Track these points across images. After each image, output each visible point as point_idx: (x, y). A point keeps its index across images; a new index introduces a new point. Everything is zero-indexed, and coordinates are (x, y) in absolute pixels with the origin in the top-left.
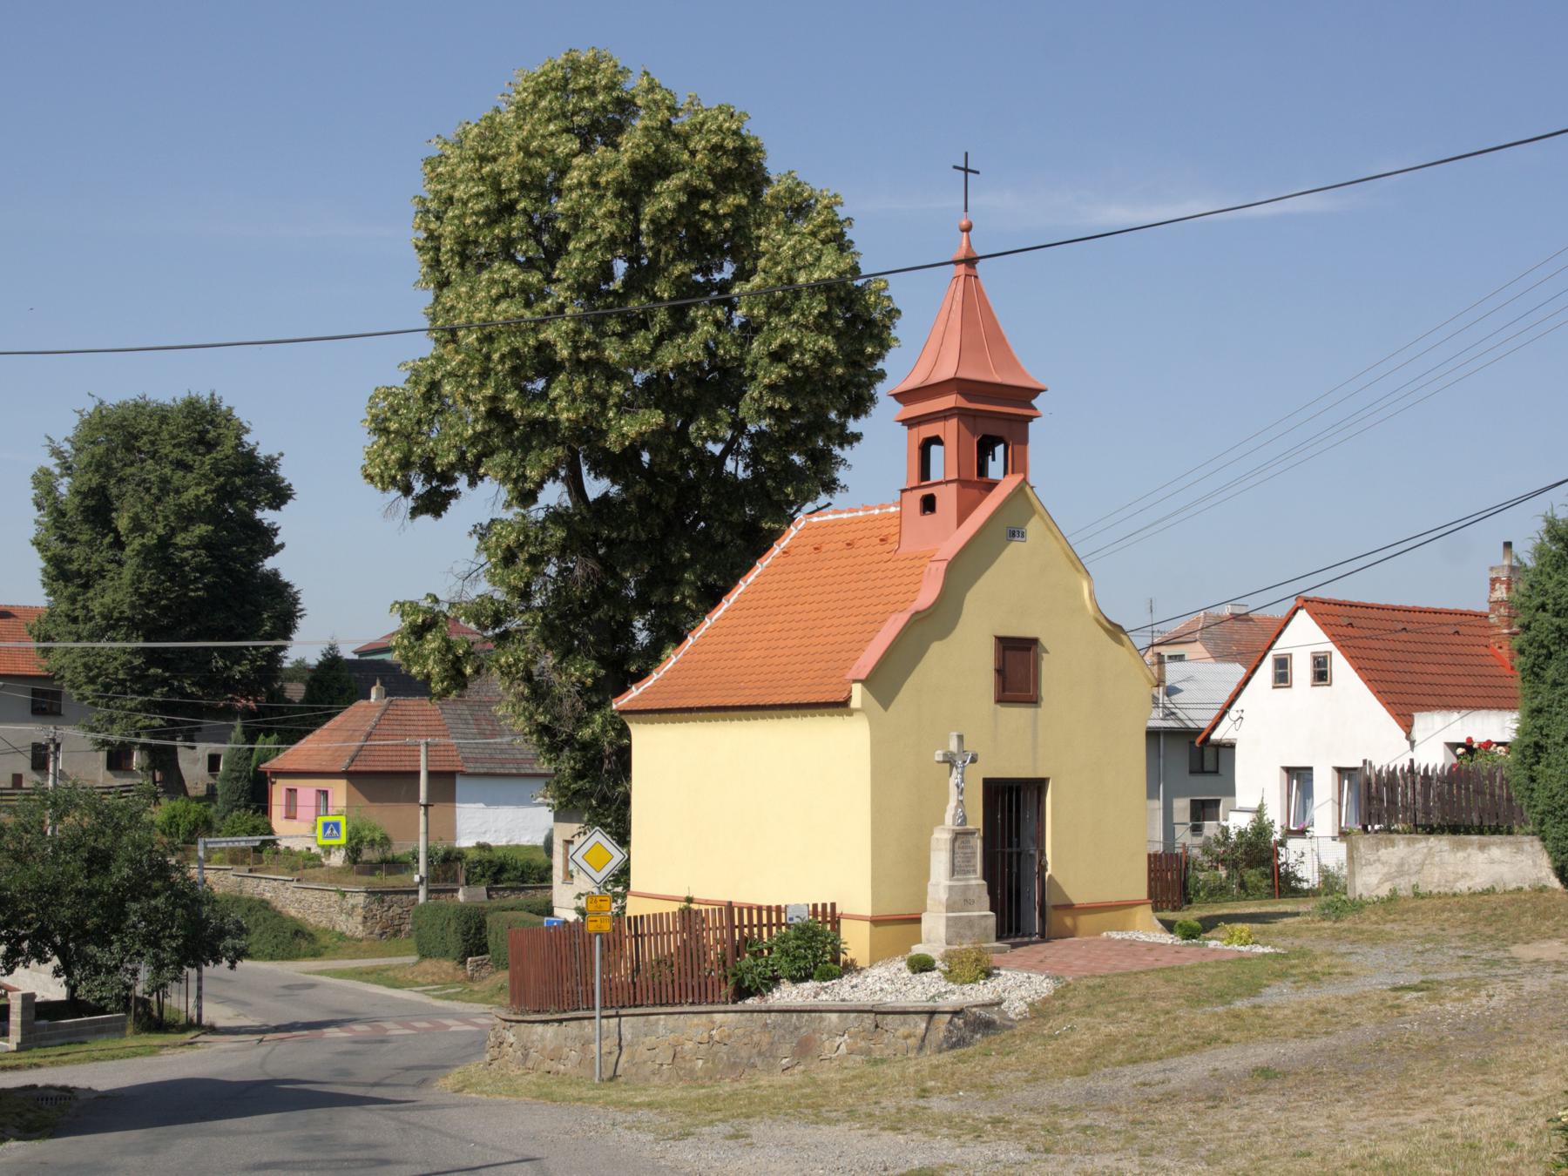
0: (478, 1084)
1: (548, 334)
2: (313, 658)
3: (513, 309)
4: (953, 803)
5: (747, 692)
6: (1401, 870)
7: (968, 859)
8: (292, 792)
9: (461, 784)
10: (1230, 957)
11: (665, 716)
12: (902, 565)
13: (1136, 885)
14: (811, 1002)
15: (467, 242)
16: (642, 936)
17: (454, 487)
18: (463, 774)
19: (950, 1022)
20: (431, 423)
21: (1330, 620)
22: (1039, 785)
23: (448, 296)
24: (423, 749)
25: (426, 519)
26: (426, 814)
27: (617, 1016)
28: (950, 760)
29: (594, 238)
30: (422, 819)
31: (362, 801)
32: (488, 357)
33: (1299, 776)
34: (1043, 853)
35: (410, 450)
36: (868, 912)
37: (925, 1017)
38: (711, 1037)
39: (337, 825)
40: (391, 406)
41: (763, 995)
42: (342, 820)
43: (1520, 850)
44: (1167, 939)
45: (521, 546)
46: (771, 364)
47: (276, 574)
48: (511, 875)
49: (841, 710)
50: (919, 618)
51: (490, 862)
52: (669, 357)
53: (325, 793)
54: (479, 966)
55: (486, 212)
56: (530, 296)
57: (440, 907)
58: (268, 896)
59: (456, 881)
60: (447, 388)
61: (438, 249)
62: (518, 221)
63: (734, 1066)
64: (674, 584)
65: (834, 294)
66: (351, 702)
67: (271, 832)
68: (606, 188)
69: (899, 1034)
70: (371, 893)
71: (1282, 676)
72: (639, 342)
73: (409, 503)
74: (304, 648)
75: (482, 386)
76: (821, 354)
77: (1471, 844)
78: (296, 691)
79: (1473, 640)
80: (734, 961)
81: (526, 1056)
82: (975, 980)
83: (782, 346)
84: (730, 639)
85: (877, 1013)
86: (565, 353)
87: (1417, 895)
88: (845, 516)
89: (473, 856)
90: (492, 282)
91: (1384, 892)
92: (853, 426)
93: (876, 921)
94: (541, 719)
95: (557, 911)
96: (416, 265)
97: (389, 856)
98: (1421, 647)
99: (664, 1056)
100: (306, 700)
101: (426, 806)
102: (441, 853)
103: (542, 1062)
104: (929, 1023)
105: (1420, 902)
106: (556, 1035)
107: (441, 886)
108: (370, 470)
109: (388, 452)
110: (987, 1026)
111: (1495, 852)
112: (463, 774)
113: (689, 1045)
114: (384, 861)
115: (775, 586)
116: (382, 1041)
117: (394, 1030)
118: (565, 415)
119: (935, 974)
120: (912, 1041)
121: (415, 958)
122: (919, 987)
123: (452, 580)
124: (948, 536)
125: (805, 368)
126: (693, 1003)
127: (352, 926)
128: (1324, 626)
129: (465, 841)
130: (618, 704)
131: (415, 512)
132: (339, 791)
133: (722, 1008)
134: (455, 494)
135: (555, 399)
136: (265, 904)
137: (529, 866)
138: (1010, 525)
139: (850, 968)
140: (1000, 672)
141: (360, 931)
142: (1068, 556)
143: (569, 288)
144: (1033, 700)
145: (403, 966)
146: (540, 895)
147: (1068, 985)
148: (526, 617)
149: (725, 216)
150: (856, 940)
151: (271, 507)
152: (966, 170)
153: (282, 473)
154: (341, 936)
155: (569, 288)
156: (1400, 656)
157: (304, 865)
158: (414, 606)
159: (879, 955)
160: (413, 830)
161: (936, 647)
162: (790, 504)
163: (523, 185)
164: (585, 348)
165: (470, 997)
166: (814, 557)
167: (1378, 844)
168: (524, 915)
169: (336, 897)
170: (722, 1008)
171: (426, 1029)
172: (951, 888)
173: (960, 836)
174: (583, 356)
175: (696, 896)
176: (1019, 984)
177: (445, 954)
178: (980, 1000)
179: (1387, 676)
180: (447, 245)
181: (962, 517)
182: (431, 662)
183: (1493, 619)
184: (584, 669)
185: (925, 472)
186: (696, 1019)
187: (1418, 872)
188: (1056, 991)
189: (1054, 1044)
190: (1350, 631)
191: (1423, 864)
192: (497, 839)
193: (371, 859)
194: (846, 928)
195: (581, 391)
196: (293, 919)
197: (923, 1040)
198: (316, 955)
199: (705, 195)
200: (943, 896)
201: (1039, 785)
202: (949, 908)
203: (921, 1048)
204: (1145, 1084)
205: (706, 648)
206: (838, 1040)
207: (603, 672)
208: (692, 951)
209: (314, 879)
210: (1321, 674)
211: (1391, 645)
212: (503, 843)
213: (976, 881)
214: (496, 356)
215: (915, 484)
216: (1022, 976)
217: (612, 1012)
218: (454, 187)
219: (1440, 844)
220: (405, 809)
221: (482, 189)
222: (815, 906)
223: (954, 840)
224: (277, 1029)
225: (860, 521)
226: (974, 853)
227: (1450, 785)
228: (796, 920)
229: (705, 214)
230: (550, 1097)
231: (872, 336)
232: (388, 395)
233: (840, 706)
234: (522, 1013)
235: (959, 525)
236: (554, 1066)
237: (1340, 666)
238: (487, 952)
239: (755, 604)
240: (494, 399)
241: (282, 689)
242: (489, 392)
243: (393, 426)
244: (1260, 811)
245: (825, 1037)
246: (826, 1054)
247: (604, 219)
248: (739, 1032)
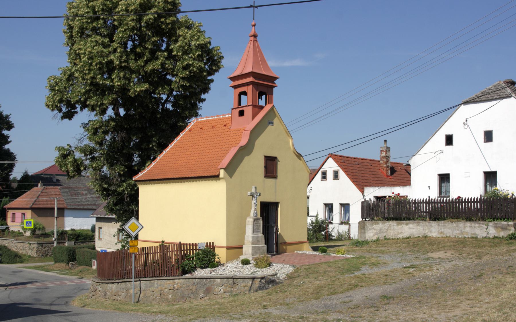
0: (90, 304)
1: (112, 57)
2: (19, 178)
3: (100, 48)
4: (253, 209)
5: (184, 173)
6: (380, 231)
7: (258, 227)
8: (14, 214)
9: (66, 212)
10: (342, 258)
11: (152, 182)
12: (232, 133)
14: (209, 275)
15: (83, 28)
16: (148, 254)
17: (76, 110)
18: (67, 209)
19: (260, 281)
20: (69, 88)
21: (338, 160)
22: (276, 204)
23: (76, 47)
24: (56, 201)
25: (66, 120)
26: (57, 220)
27: (139, 281)
28: (252, 195)
29: (127, 28)
30: (55, 221)
31: (36, 216)
32: (91, 64)
33: (329, 207)
34: (277, 226)
35: (63, 96)
36: (225, 244)
37: (251, 280)
38: (174, 287)
39: (30, 222)
40: (56, 82)
41: (191, 273)
42: (32, 221)
43: (419, 225)
44: (315, 253)
45: (100, 127)
46: (183, 70)
47: (8, 150)
48: (82, 238)
49: (216, 178)
50: (242, 149)
51: (75, 234)
52: (149, 68)
53: (24, 214)
54: (73, 265)
55: (90, 18)
56: (105, 46)
57: (61, 247)
58: (6, 245)
59: (65, 240)
60: (77, 74)
61: (72, 32)
62: (101, 22)
63: (183, 297)
64: (150, 142)
65: (204, 50)
66: (32, 188)
67: (7, 225)
68: (131, 12)
69: (242, 285)
70: (39, 244)
71: (324, 176)
72: (140, 62)
73: (61, 114)
74: (17, 174)
75: (89, 73)
76: (199, 68)
77: (403, 223)
78: (15, 185)
79: (375, 168)
80: (182, 262)
81: (105, 294)
82: (266, 267)
83: (187, 65)
84: (173, 157)
85: (234, 279)
86: (118, 63)
87: (385, 239)
88: (210, 118)
89: (70, 232)
90: (92, 41)
91: (375, 238)
92: (203, 96)
93: (228, 248)
94: (105, 186)
95: (97, 248)
96: (64, 38)
97: (44, 233)
98: (363, 169)
99: (157, 294)
100: (17, 188)
101: (57, 218)
102: (60, 232)
103: (112, 296)
104: (253, 281)
105: (387, 241)
106: (117, 287)
107: (60, 241)
108: (49, 104)
109: (55, 97)
110: (273, 282)
111: (411, 226)
112: (67, 209)
113: (166, 290)
114: (42, 234)
115: (188, 140)
116: (46, 288)
117: (49, 285)
118: (117, 83)
119: (251, 265)
120: (247, 288)
121: (53, 263)
122: (247, 270)
123: (75, 140)
124: (249, 123)
125: (194, 72)
126: (166, 276)
127: (33, 253)
128: (337, 162)
129: (67, 228)
130: (135, 178)
131: (63, 118)
132: (29, 213)
133: (178, 278)
134: (76, 113)
135: (114, 79)
136: (5, 247)
137: (87, 235)
138: (268, 120)
139: (219, 264)
140: (266, 167)
141: (35, 255)
142: (286, 131)
143: (119, 43)
144: (275, 177)
145: (49, 265)
146: (90, 244)
147: (298, 268)
148: (101, 151)
149: (169, 23)
150: (221, 254)
151: (7, 130)
153: (11, 120)
154: (30, 256)
155: (119, 43)
156: (358, 171)
157: (17, 235)
158: (63, 148)
159: (229, 259)
160: (52, 225)
161: (246, 158)
162: (186, 117)
163: (103, 10)
164: (124, 62)
165: (71, 274)
166: (200, 131)
167: (373, 224)
168: (87, 249)
169: (28, 245)
170: (178, 278)
171: (59, 285)
172: (253, 237)
173: (256, 220)
174: (123, 65)
175: (166, 241)
176: (280, 269)
177: (63, 261)
178: (269, 274)
179: (355, 177)
180: (76, 29)
181: (254, 117)
182: (69, 166)
183: (381, 162)
184: (119, 169)
185: (240, 103)
186: (168, 282)
187: (386, 232)
188: (295, 270)
189: (299, 289)
190: (344, 164)
191: (387, 230)
192: (77, 228)
193: (39, 234)
194: (217, 251)
195: (122, 76)
196: (14, 252)
197: (251, 287)
198: (22, 262)
199: (163, 17)
200: (251, 240)
201: (276, 204)
202: (253, 244)
203: (250, 290)
204: (345, 302)
205: (164, 160)
206: (220, 288)
207: (126, 170)
208: (165, 258)
209: (21, 239)
210: (336, 176)
211: (355, 168)
212: (79, 229)
213: (261, 234)
214: (94, 64)
215: (237, 107)
216: (281, 265)
217: (138, 279)
218: (78, 10)
219: (393, 223)
220: (50, 219)
221: (89, 10)
222: (207, 243)
223: (254, 221)
224: (11, 285)
225: (216, 120)
227: (396, 205)
228: (202, 248)
229: (162, 23)
230: (119, 309)
231: (215, 64)
232: (55, 78)
233: (216, 177)
234: (105, 280)
235: (252, 120)
236: (116, 298)
237: (342, 174)
238: (76, 260)
239: (181, 146)
240: (93, 78)
241: (10, 184)
242: (92, 75)
243: (57, 88)
244: (317, 217)
245: (215, 287)
246: (216, 293)
247: (130, 21)
248: (184, 286)
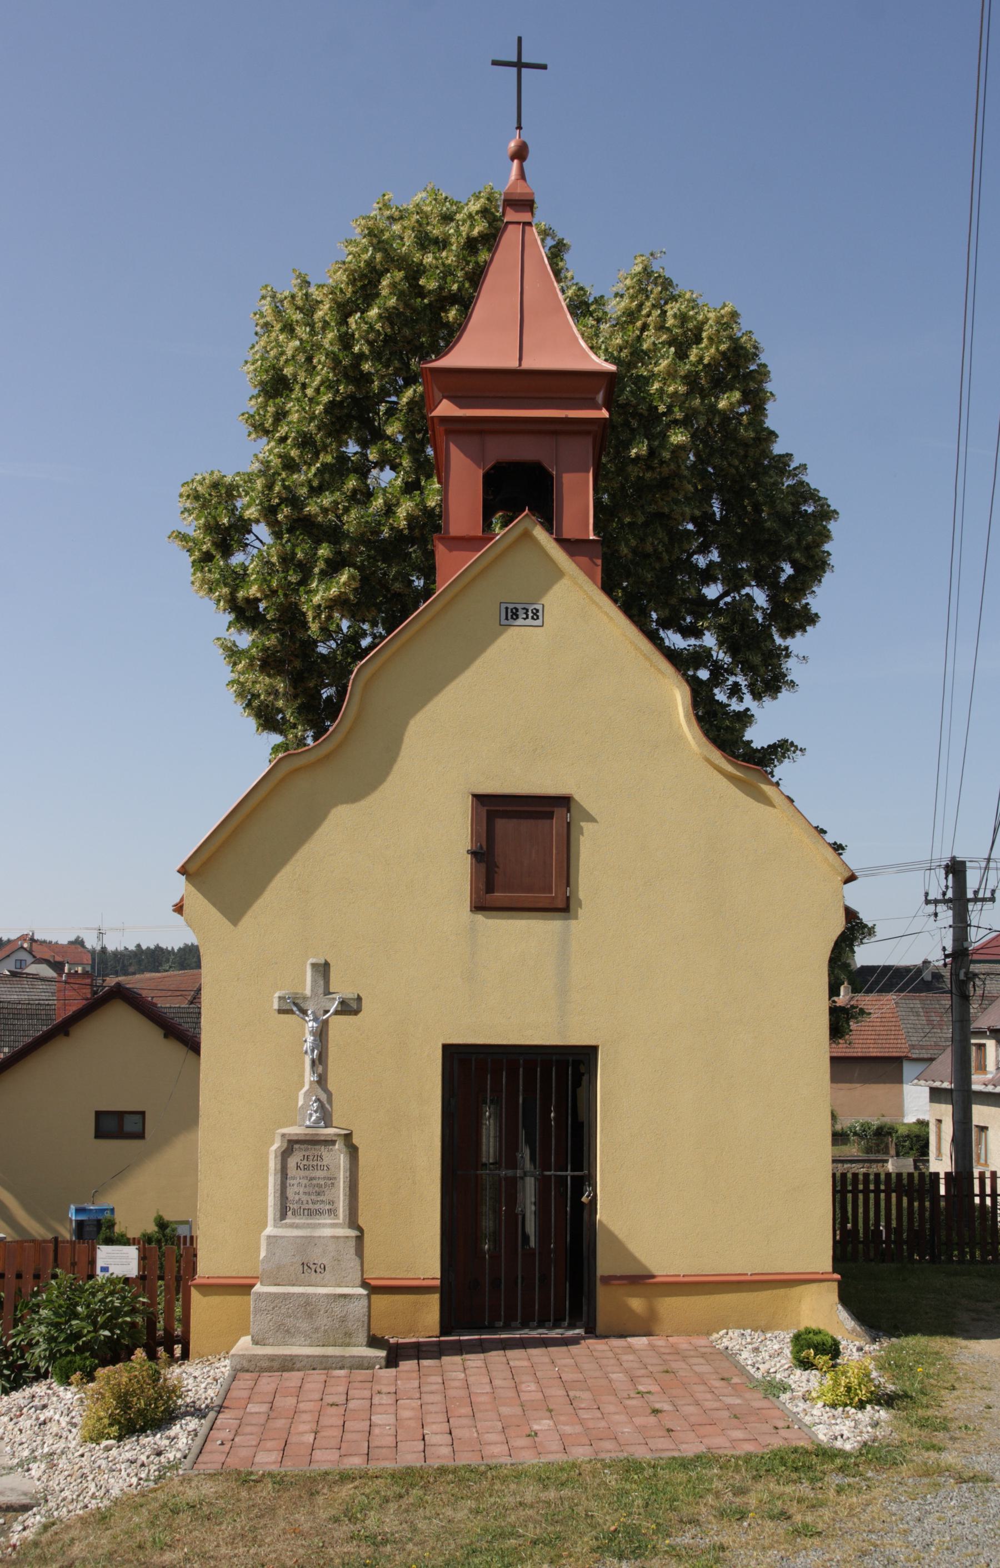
13: (808, 1240)
107: (872, 1157)
152: (519, 65)
226: (332, 1180)
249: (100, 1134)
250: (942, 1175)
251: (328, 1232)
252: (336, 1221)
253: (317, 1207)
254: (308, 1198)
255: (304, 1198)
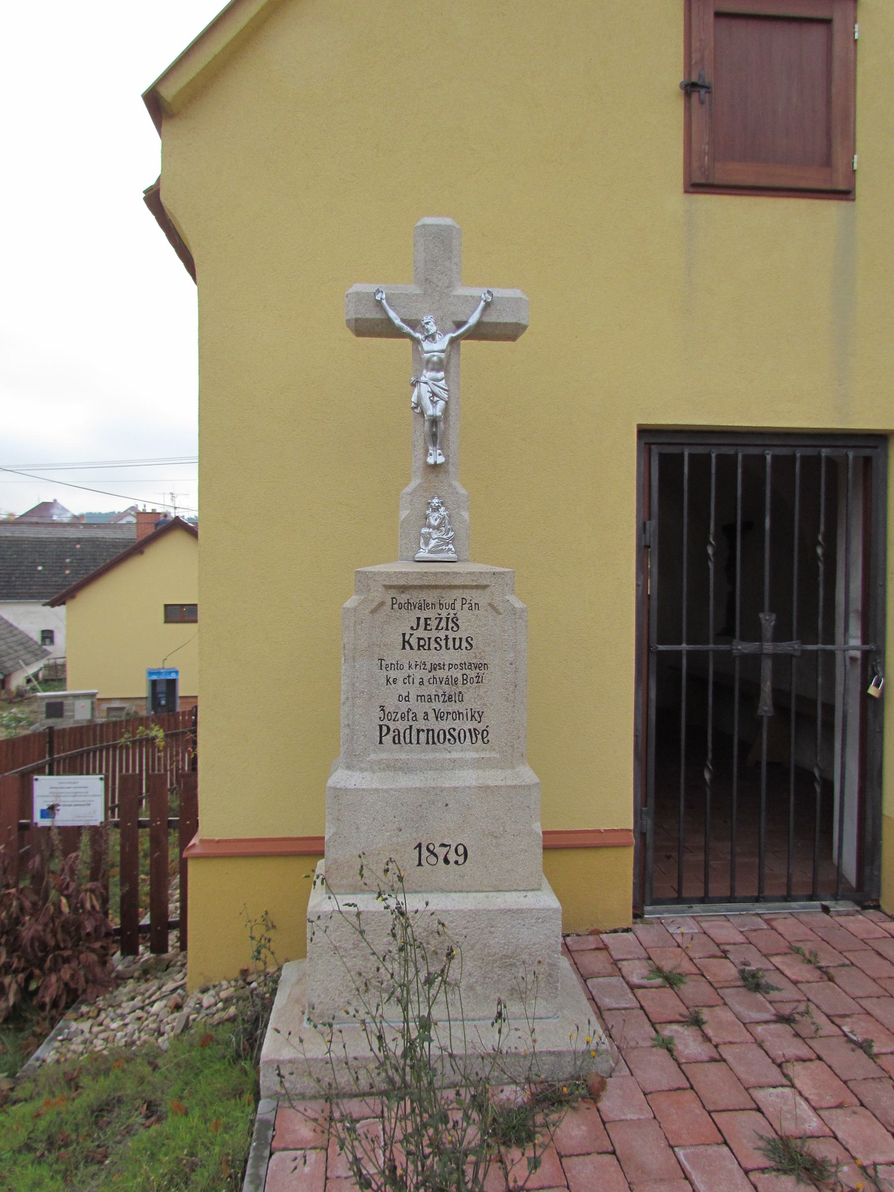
249: (168, 620)
250: (684, 652)
251: (469, 778)
252: (487, 755)
253: (446, 725)
254: (427, 707)
255: (420, 708)
